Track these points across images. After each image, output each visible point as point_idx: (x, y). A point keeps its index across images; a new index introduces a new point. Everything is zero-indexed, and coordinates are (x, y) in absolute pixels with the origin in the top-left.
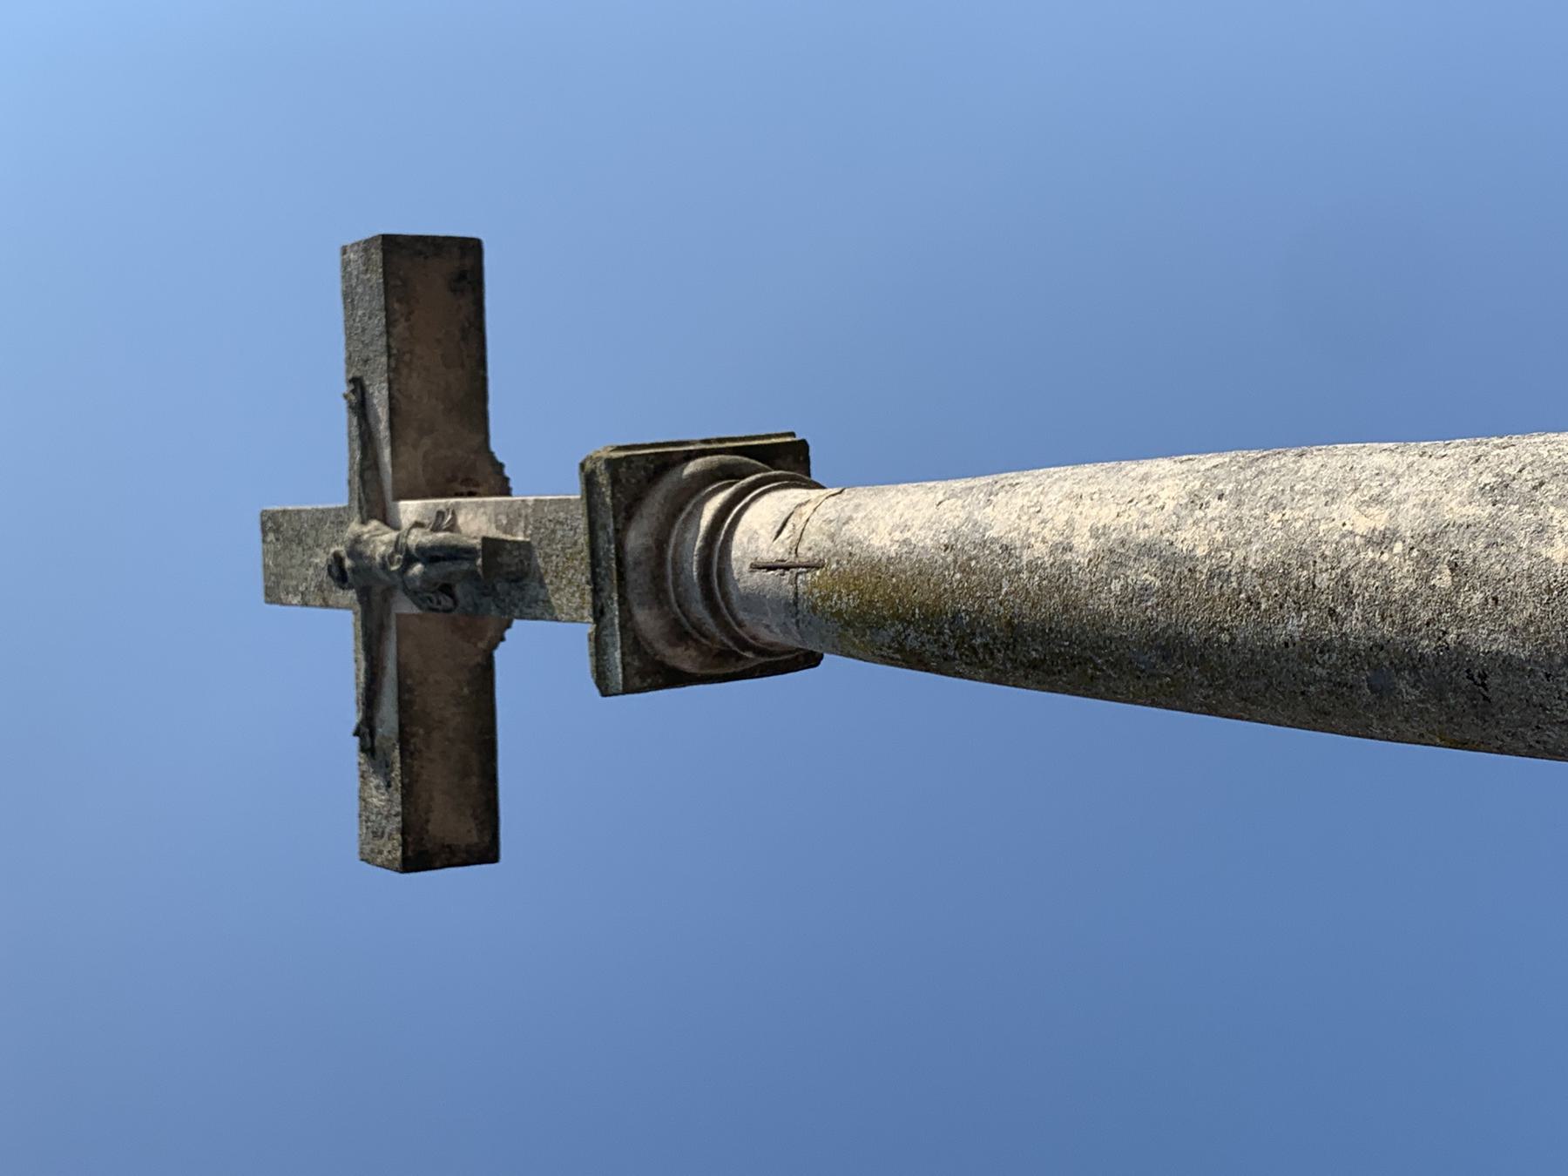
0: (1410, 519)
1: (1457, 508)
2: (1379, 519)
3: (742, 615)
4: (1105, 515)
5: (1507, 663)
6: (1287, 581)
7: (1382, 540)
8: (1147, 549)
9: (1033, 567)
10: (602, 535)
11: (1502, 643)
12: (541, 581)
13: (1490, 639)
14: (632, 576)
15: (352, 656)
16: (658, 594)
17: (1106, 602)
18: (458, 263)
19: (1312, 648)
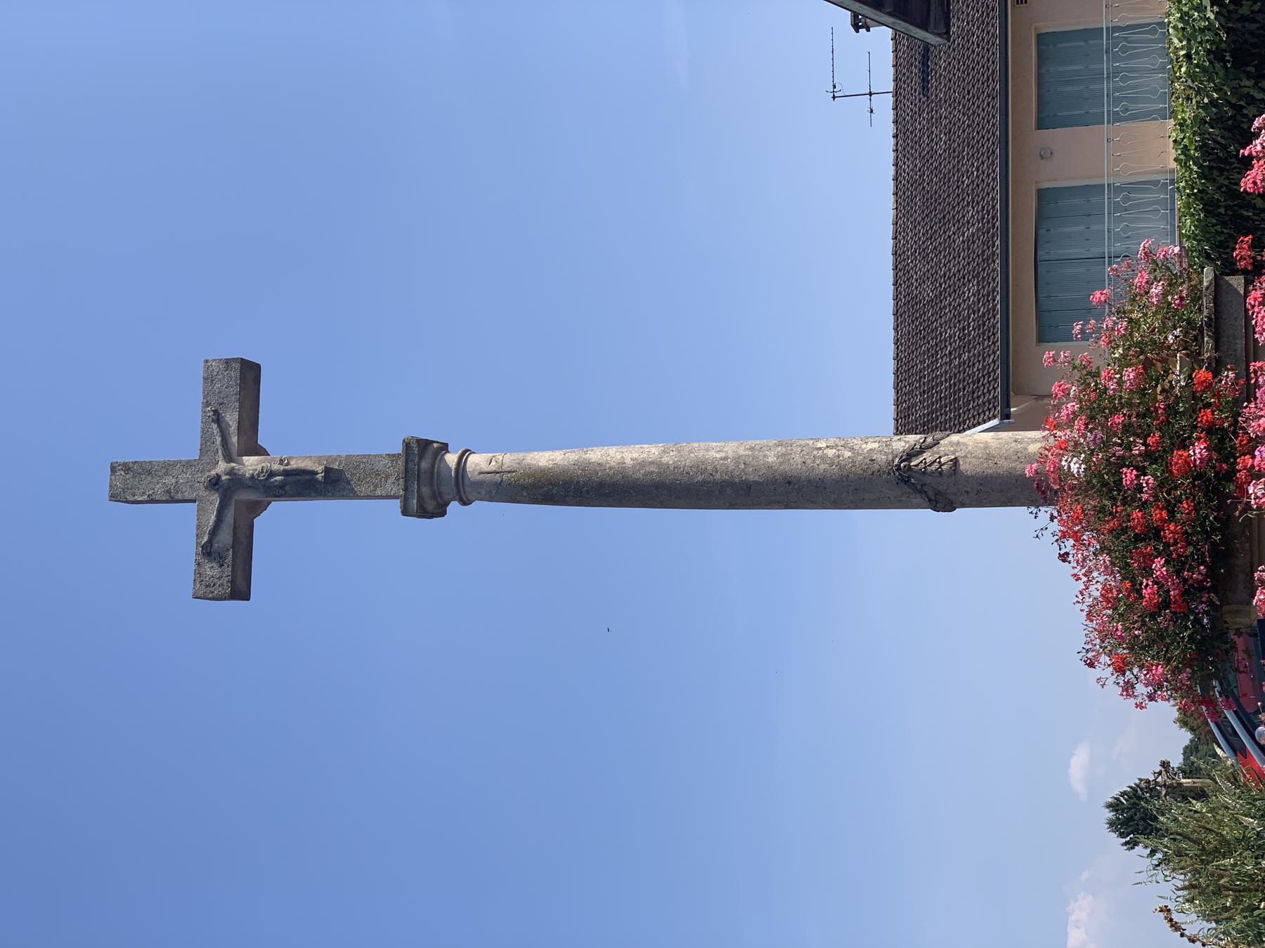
0: (730, 454)
1: (741, 452)
2: (723, 455)
3: (468, 489)
4: (635, 455)
5: (757, 483)
6: (699, 467)
7: (726, 458)
8: (652, 463)
9: (610, 468)
10: (410, 464)
11: (756, 478)
12: (348, 482)
13: (751, 478)
14: (422, 476)
15: (194, 557)
16: (431, 483)
17: (639, 476)
18: (249, 373)
19: (704, 482)
